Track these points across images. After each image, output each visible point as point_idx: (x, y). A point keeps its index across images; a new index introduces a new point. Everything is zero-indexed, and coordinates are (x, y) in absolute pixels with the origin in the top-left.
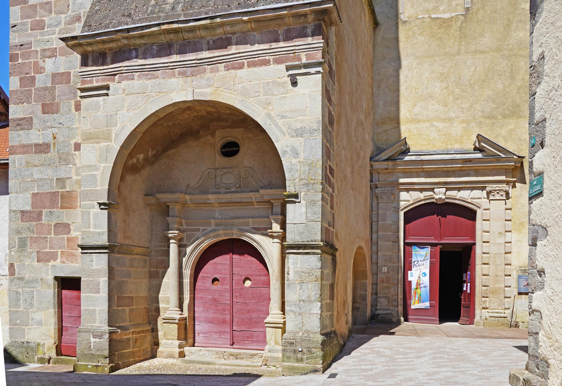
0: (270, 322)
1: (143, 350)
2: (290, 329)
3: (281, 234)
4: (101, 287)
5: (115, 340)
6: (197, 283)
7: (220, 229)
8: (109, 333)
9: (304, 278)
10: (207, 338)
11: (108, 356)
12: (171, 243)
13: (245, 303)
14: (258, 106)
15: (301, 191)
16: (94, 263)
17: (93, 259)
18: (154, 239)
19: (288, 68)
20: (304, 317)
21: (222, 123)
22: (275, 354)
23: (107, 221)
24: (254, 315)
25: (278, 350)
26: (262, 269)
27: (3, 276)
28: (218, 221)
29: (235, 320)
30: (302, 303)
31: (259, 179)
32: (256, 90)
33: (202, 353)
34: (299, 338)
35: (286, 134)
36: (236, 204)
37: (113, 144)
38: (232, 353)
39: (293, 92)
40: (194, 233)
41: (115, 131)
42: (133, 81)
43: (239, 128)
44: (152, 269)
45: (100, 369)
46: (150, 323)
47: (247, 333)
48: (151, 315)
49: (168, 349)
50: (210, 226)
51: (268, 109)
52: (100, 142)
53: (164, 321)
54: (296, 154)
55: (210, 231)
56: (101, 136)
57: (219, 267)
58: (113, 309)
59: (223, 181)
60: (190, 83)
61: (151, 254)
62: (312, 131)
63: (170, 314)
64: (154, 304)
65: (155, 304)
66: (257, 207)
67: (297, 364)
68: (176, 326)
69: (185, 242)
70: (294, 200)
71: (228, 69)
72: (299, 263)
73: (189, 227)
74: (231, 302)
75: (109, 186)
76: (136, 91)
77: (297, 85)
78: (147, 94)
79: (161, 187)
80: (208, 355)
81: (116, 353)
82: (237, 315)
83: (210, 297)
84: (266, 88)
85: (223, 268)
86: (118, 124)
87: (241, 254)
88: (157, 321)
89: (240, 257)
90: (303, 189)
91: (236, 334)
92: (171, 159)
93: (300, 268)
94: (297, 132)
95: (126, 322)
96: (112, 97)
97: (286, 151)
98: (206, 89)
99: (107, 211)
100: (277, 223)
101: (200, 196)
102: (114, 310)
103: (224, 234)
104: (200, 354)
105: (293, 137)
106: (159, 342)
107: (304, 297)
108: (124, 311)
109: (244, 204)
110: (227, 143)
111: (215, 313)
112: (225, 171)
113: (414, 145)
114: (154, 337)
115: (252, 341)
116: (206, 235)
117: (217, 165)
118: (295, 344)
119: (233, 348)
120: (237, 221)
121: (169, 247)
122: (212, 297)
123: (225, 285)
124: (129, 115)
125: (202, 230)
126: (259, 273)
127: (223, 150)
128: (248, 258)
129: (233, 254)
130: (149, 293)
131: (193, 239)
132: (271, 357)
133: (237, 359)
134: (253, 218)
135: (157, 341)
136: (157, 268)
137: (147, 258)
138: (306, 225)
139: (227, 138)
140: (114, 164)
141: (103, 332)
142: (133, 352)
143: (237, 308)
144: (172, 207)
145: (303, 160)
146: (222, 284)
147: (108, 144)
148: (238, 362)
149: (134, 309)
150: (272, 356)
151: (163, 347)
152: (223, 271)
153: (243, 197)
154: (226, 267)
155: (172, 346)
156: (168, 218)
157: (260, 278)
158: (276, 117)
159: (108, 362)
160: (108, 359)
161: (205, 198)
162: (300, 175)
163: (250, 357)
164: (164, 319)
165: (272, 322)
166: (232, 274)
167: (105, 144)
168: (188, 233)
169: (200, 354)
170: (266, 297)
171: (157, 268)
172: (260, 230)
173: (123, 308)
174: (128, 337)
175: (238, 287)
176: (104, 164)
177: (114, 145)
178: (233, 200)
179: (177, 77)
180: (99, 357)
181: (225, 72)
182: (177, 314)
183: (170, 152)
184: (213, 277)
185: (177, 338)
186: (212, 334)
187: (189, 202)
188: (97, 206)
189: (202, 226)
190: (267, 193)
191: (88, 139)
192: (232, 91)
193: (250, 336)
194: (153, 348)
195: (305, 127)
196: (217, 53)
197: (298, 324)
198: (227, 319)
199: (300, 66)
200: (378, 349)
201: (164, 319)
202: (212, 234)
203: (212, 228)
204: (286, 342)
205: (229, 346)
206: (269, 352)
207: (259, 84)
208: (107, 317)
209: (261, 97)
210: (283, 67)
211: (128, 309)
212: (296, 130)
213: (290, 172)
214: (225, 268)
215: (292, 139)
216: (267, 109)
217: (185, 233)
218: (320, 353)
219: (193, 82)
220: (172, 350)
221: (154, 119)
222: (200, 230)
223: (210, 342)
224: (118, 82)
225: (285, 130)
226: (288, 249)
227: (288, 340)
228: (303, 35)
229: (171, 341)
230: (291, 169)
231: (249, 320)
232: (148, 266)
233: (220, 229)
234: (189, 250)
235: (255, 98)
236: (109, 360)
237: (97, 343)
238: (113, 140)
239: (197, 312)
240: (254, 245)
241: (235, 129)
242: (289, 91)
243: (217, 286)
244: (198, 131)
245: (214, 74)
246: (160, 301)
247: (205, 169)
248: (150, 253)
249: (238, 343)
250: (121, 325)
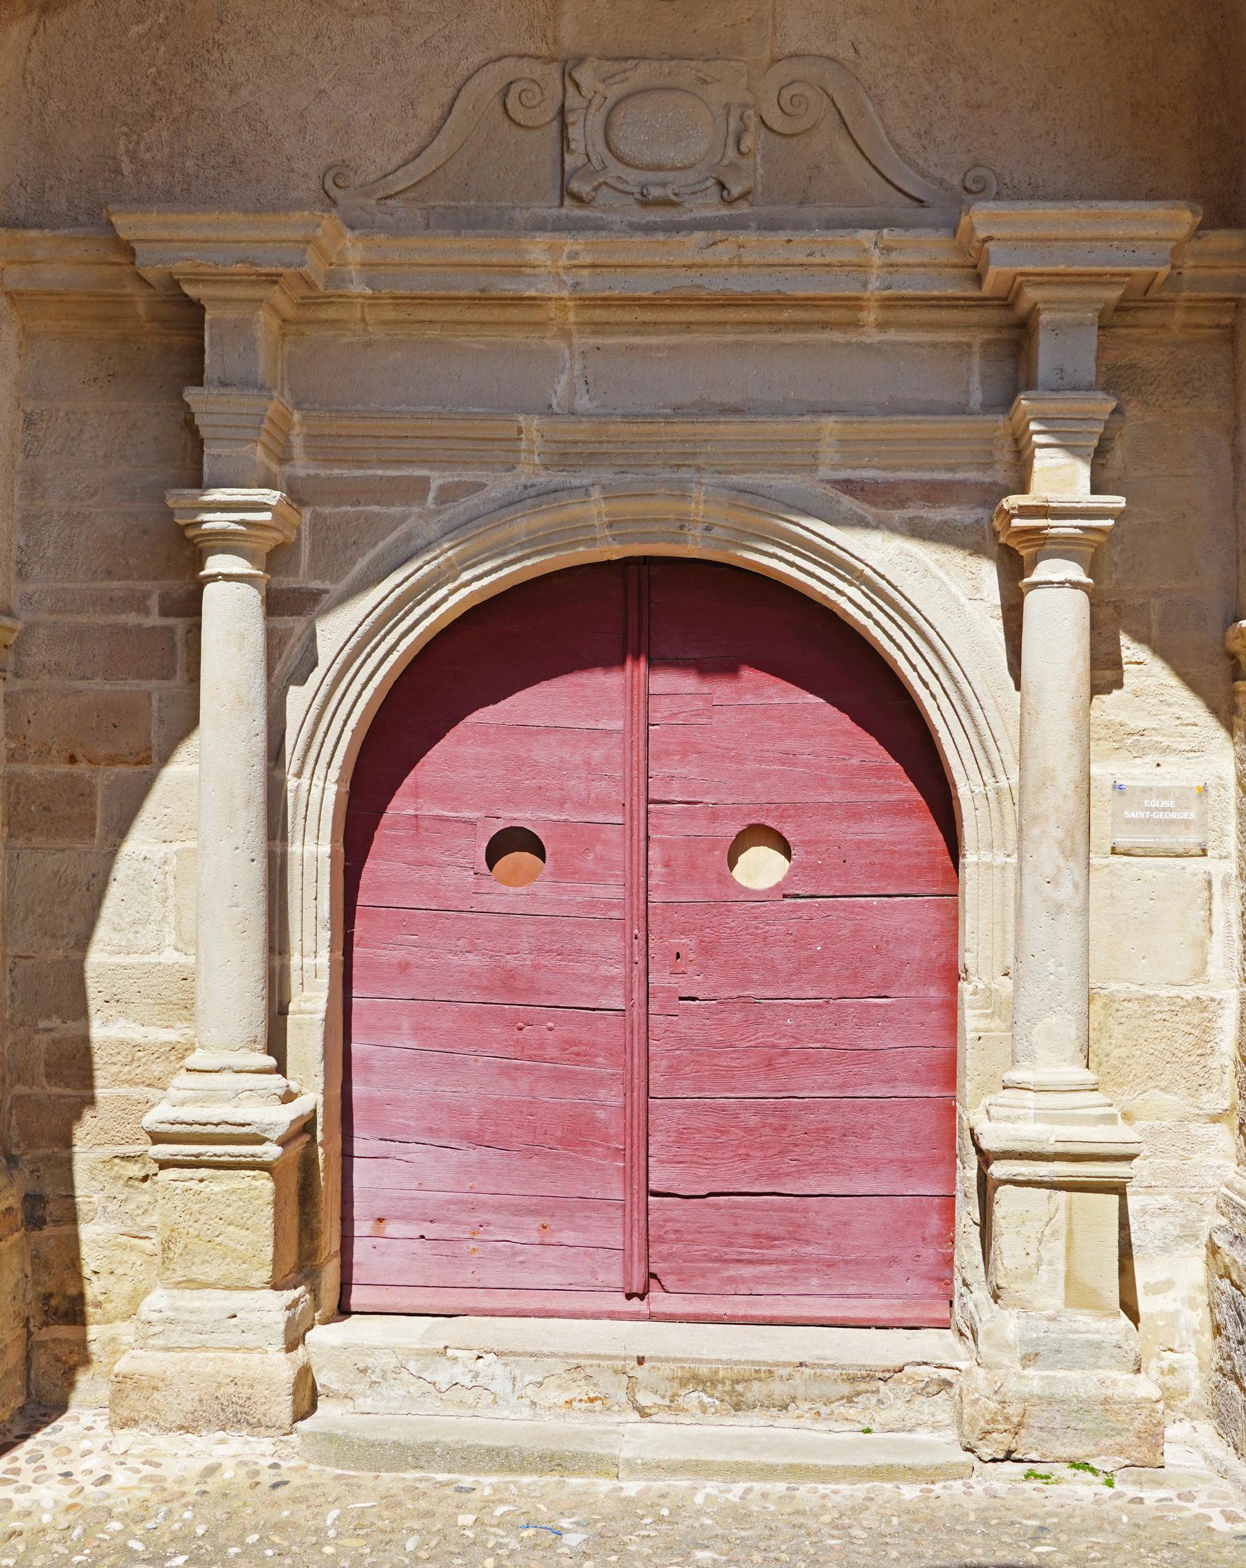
0: (1036, 1148)
3: (1110, 522)
6: (369, 864)
7: (586, 490)
10: (445, 1249)
12: (213, 578)
13: (744, 1001)
18: (50, 553)
22: (1075, 1375)
25: (1098, 1346)
26: (879, 771)
27: (188, 1070)
29: (666, 1118)
31: (898, 147)
36: (717, 315)
38: (703, 1370)
40: (376, 509)
47: (755, 1208)
48: (18, 1098)
49: (204, 1363)
57: (543, 753)
59: (624, 149)
63: (212, 1096)
64: (42, 1024)
65: (55, 1022)
68: (264, 1184)
69: (301, 579)
73: (336, 471)
74: (638, 995)
79: (118, 171)
80: (501, 1386)
83: (472, 960)
85: (578, 759)
88: (68, 1144)
89: (705, 688)
91: (677, 1213)
100: (1072, 449)
104: (443, 1379)
106: (81, 1296)
109: (786, 315)
111: (506, 1072)
112: (641, 75)
114: (40, 1263)
115: (796, 1260)
119: (652, 1317)
120: (730, 429)
121: (191, 607)
123: (593, 878)
125: (442, 489)
126: (853, 797)
128: (771, 691)
129: (653, 665)
131: (371, 554)
132: (1051, 1400)
133: (737, 1407)
134: (843, 412)
135: (72, 1291)
136: (72, 760)
143: (683, 1040)
144: (231, 315)
146: (561, 873)
150: (1060, 1390)
152: (576, 786)
153: (801, 258)
154: (597, 755)
155: (237, 1339)
156: (192, 395)
157: (857, 828)
163: (846, 1389)
164: (157, 1138)
166: (648, 802)
168: (327, 510)
169: (443, 1379)
170: (903, 964)
172: (901, 503)
178: (715, 284)
182: (266, 1095)
184: (500, 825)
185: (266, 1274)
186: (490, 1217)
187: (357, 288)
190: (1027, 232)
193: (781, 1230)
194: (42, 1344)
198: (601, 1114)
201: (157, 1138)
202: (521, 526)
203: (523, 480)
205: (618, 1302)
214: (587, 763)
222: (426, 489)
223: (466, 1277)
229: (217, 1302)
231: (775, 1121)
233: (586, 490)
239: (368, 1069)
246: (93, 1006)
249: (684, 1277)
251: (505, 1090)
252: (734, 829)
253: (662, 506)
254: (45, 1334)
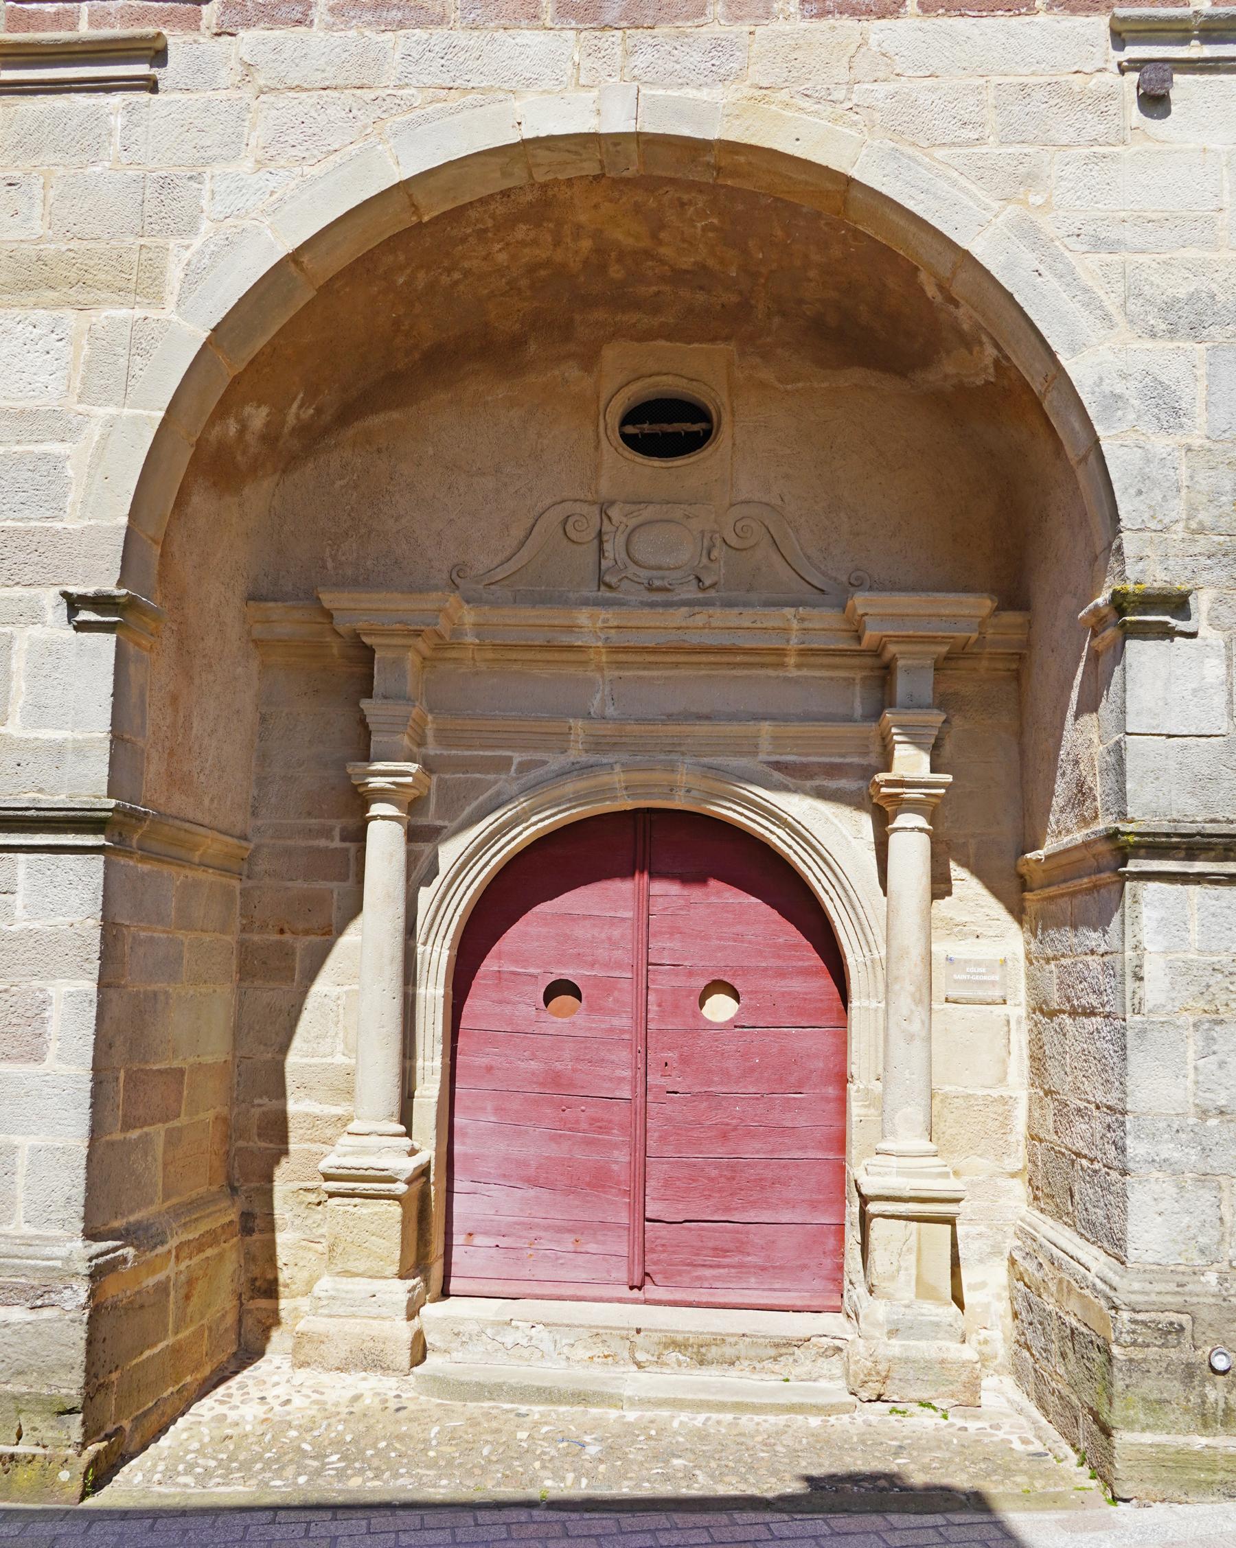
0: (897, 1193)
1: (210, 1329)
2: (1150, 1257)
3: (943, 791)
4: (53, 1028)
5: (114, 1307)
6: (469, 1001)
7: (611, 766)
8: (91, 1276)
9: (1223, 997)
10: (512, 1254)
11: (78, 1402)
12: (374, 818)
14: (972, 187)
15: (1200, 581)
16: (19, 900)
17: (12, 879)
18: (273, 800)
19: (1119, 38)
20: (1226, 1195)
21: (632, 317)
22: (923, 1344)
23: (108, 687)
24: (752, 1150)
25: (937, 1325)
26: (795, 947)
28: (607, 729)
29: (657, 1171)
30: (1213, 1122)
31: (808, 558)
32: (966, 118)
33: (519, 1334)
34: (1212, 1300)
35: (1119, 318)
36: (695, 658)
37: (169, 313)
38: (679, 1338)
39: (1149, 138)
40: (478, 776)
41: (187, 255)
42: (301, 29)
43: (714, 340)
44: (256, 938)
45: (23, 1475)
46: (234, 1190)
47: (714, 1230)
48: (240, 1149)
49: (354, 1326)
50: (564, 751)
51: (1024, 202)
52: (98, 302)
53: (333, 1186)
55: (563, 774)
56: (102, 276)
57: (582, 932)
58: (107, 1142)
59: (638, 556)
60: (618, 59)
61: (257, 869)
63: (364, 1151)
64: (257, 1101)
65: (265, 1100)
66: (794, 673)
67: (1204, 1441)
68: (395, 1209)
69: (430, 818)
70: (1173, 622)
72: (1194, 926)
73: (453, 752)
74: (640, 1090)
75: (133, 515)
76: (319, 75)
77: (1167, 112)
78: (379, 92)
79: (324, 567)
80: (547, 1346)
81: (114, 1376)
82: (669, 1150)
83: (534, 1065)
84: (1016, 109)
85: (603, 936)
86: (205, 226)
87: (693, 877)
88: (270, 1179)
89: (686, 892)
90: (1206, 576)
91: (663, 1233)
92: (379, 451)
93: (1200, 951)
94: (1172, 317)
95: (152, 1202)
96: (177, 96)
97: (1119, 397)
98: (705, 90)
99: (112, 638)
101: (534, 613)
102: (111, 1144)
103: (626, 788)
104: (509, 1340)
105: (1153, 336)
106: (276, 1280)
107: (1224, 1094)
108: (146, 1140)
109: (739, 659)
110: (657, 401)
111: (553, 1138)
112: (649, 513)
114: (250, 1258)
115: (741, 1266)
117: (605, 487)
118: (1188, 1333)
121: (359, 836)
122: (542, 1066)
123: (613, 1013)
124: (271, 185)
125: (520, 764)
126: (780, 963)
127: (630, 429)
128: (727, 894)
130: (235, 1048)
131: (474, 804)
132: (907, 1361)
133: (701, 1363)
135: (270, 1276)
136: (282, 931)
137: (236, 885)
138: (1227, 744)
139: (657, 379)
140: (168, 411)
141: (54, 1269)
142: (176, 1351)
143: (669, 1120)
144: (390, 655)
145: (1207, 443)
146: (591, 1009)
147: (139, 313)
148: (710, 1376)
149: (180, 1130)
150: (913, 1354)
151: (326, 1311)
152: (602, 953)
153: (749, 624)
154: (616, 933)
155: (375, 1311)
156: (365, 704)
157: (783, 983)
158: (1067, 240)
159: (77, 1434)
160: (80, 1417)
161: (556, 622)
162: (1192, 509)
163: (772, 1352)
164: (328, 1177)
165: (907, 1193)
166: (648, 964)
167: (123, 313)
168: (447, 776)
170: (811, 1072)
171: (282, 931)
173: (146, 1129)
174: (160, 1277)
175: (673, 1024)
176: (112, 410)
177: (174, 317)
178: (694, 639)
179: (549, 24)
180: (20, 1411)
181: (804, 25)
183: (376, 421)
184: (553, 978)
186: (542, 1234)
187: (470, 639)
188: (56, 612)
189: (524, 748)
190: (890, 611)
191: (27, 286)
192: (839, 109)
193: (731, 1246)
194: (250, 1311)
195: (1213, 297)
197: (1193, 1231)
198: (615, 1167)
199: (1187, 30)
201: (328, 1177)
203: (572, 759)
204: (1144, 1323)
205: (625, 1292)
206: (893, 1333)
207: (977, 90)
208: (82, 1188)
209: (992, 148)
210: (1099, 25)
211: (163, 1133)
212: (1168, 307)
213: (1140, 492)
214: (609, 939)
215: (1149, 344)
216: (1020, 201)
217: (434, 778)
219: (633, 53)
220: (377, 1328)
221: (397, 220)
222: (510, 764)
223: (525, 1273)
224: (215, 30)
225: (1111, 304)
226: (1137, 857)
227: (1153, 1315)
229: (362, 1286)
230: (1145, 478)
232: (238, 922)
233: (611, 766)
234: (449, 853)
235: (958, 150)
236: (84, 1423)
237: (15, 1333)
238: (171, 300)
239: (464, 1135)
240: (774, 839)
241: (696, 345)
242: (1128, 135)
244: (517, 343)
245: (747, 29)
247: (549, 501)
248: (250, 860)
249: (668, 1276)
250: (132, 1219)
251: (553, 1150)
252: (702, 983)
253: (658, 776)
254: (252, 1305)
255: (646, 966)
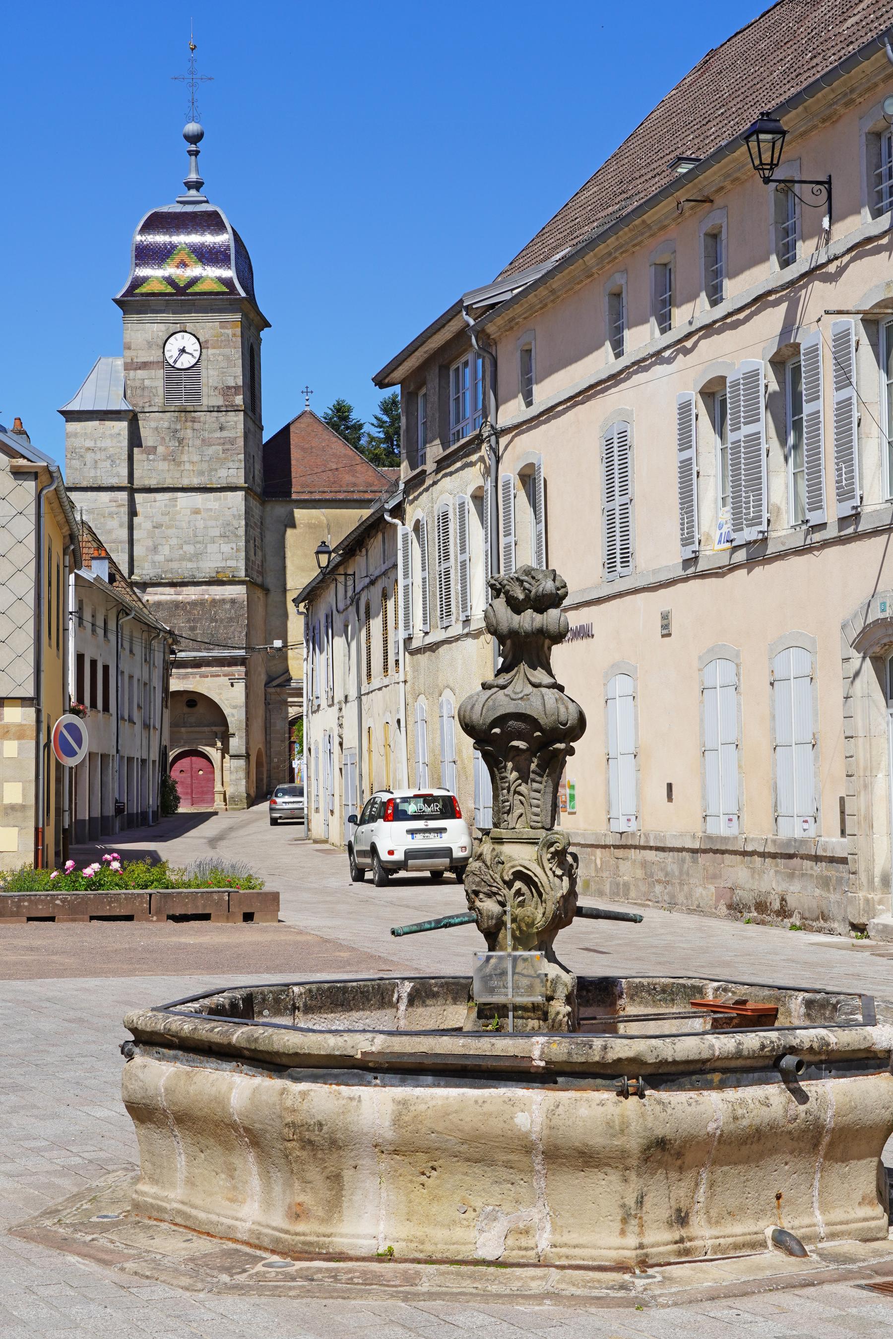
54: (233, 715)
62: (241, 707)
71: (201, 677)
113: (294, 677)
116: (177, 747)
196: (195, 670)
200: (350, 1241)
218: (245, 801)
228: (236, 665)
243: (183, 775)
255: (192, 768)
